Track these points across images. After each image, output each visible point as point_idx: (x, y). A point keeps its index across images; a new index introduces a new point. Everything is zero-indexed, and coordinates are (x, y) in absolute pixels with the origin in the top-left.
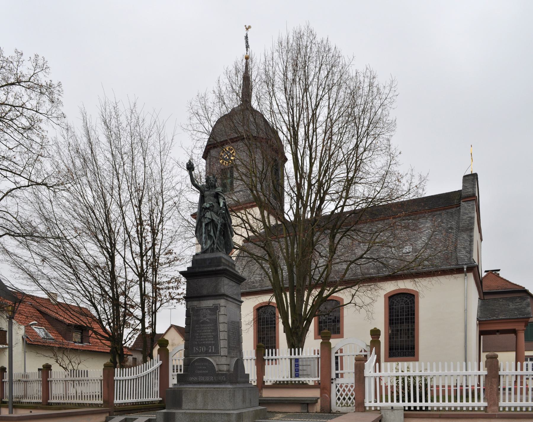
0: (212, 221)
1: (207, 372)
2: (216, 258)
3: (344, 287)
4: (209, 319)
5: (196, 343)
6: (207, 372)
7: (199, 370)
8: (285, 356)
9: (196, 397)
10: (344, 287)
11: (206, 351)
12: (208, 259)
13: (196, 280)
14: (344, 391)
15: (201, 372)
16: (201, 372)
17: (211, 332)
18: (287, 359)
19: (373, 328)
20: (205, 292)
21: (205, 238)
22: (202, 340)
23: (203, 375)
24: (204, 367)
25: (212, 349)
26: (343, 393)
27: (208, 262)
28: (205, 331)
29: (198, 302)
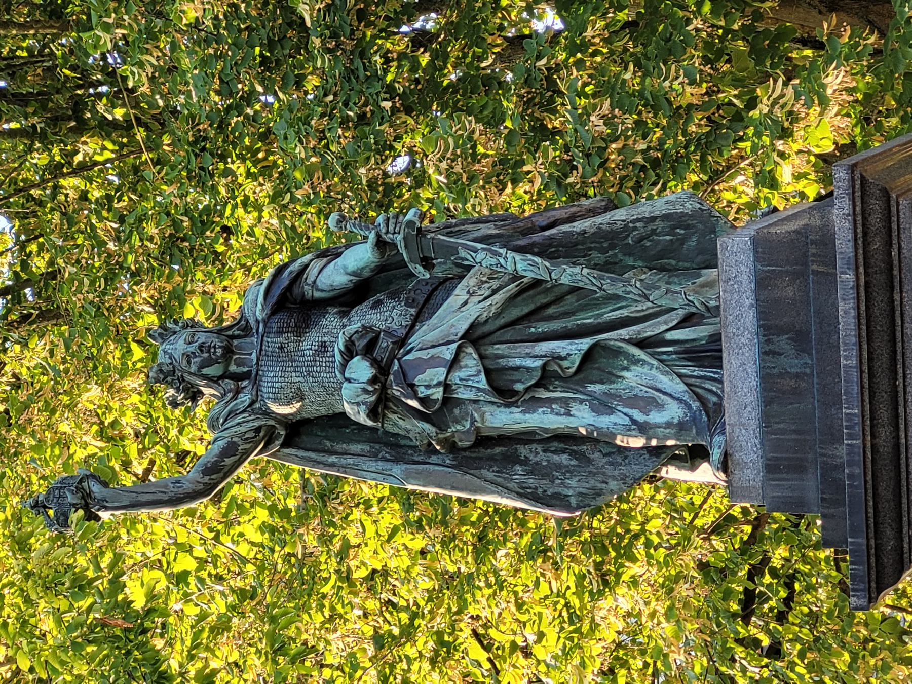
0: (475, 336)
2: (762, 283)
12: (767, 353)
27: (792, 362)
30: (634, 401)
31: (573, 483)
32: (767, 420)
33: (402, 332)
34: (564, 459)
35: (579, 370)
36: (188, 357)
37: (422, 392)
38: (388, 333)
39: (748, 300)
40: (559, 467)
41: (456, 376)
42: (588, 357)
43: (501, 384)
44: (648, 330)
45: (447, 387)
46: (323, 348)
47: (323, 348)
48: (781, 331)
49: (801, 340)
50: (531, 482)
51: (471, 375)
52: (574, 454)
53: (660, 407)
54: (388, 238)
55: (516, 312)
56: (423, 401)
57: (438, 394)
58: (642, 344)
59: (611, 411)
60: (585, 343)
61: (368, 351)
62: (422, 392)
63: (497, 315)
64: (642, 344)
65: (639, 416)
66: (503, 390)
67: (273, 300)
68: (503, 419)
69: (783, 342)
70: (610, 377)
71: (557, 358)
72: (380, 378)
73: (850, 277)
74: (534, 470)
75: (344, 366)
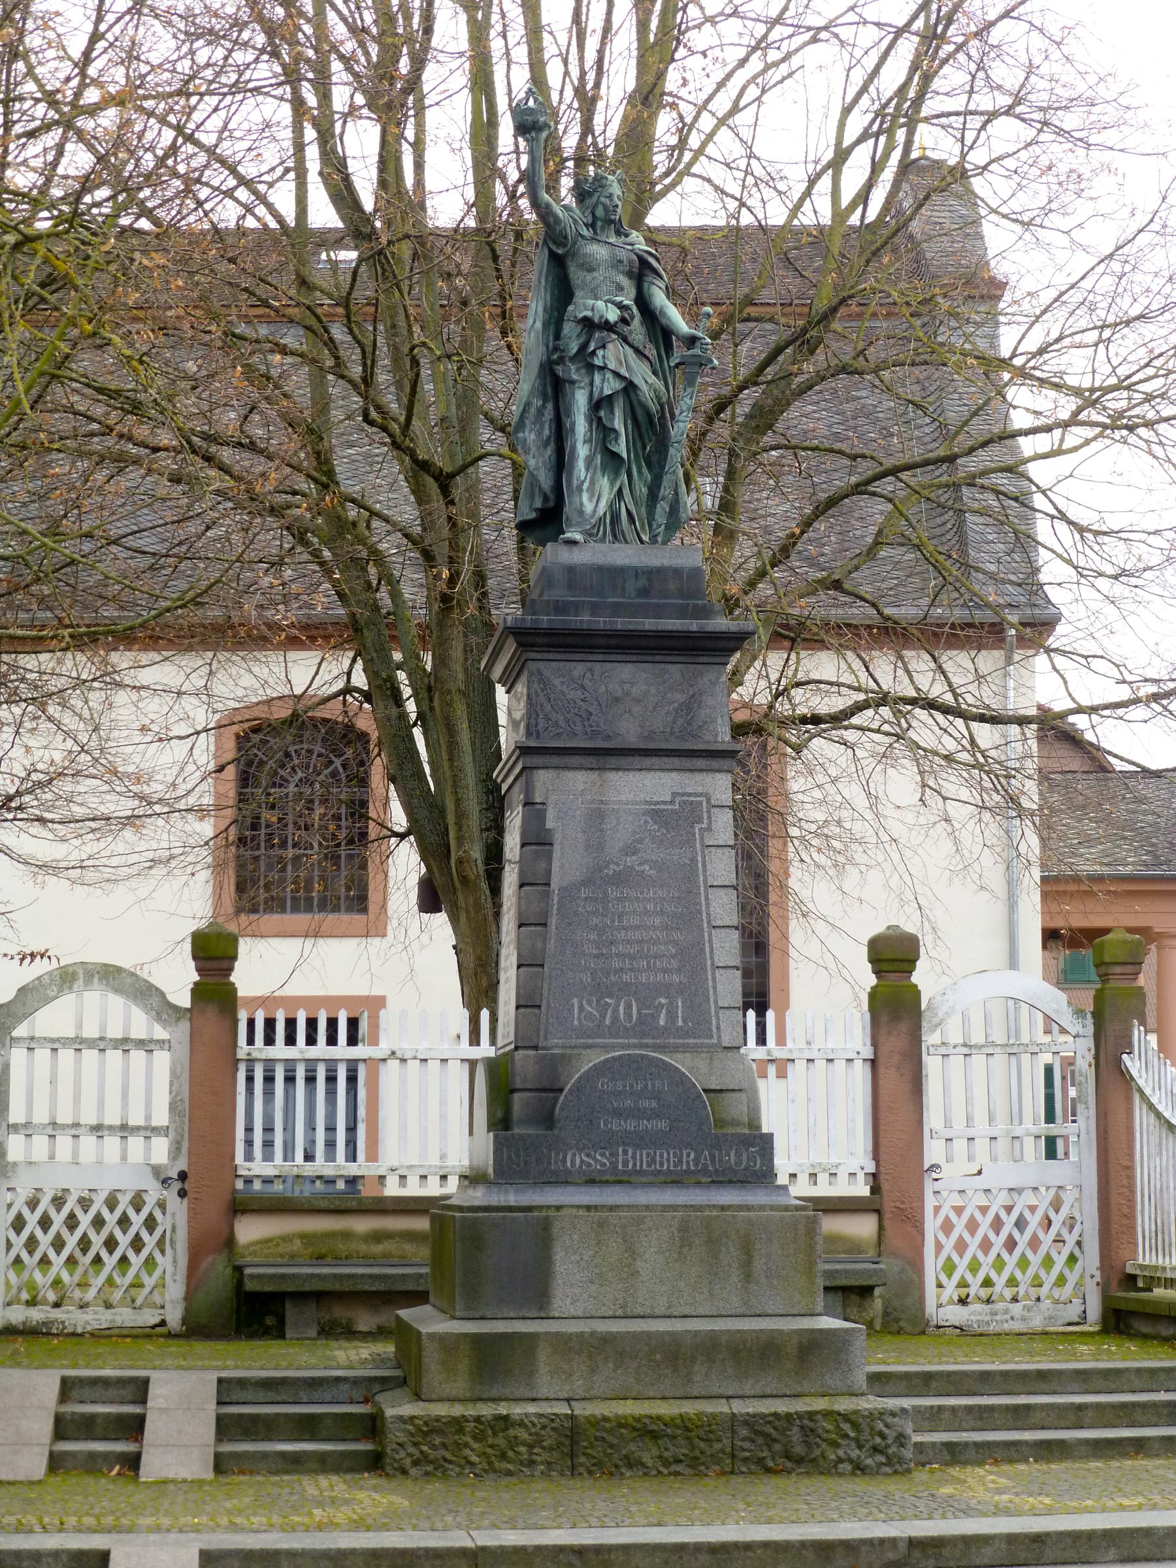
0: (630, 388)
1: (662, 1125)
2: (677, 571)
3: (1110, 758)
4: (654, 865)
5: (586, 978)
6: (662, 1125)
7: (618, 1114)
8: (445, 1048)
9: (632, 1252)
10: (1110, 758)
11: (641, 1021)
12: (637, 572)
13: (579, 669)
14: (45, 1223)
15: (630, 1125)
16: (630, 1125)
17: (666, 927)
18: (858, 1064)
19: (879, 928)
20: (629, 732)
21: (589, 462)
22: (616, 963)
23: (640, 1140)
24: (646, 1104)
25: (671, 1015)
26: (65, 1233)
27: (632, 586)
28: (635, 921)
29: (593, 776)
30: (592, 483)
31: (533, 436)
32: (600, 569)
33: (630, 339)
34: (546, 432)
35: (607, 449)
36: (610, 196)
37: (600, 353)
38: (631, 332)
39: (666, 562)
40: (542, 428)
41: (609, 375)
42: (616, 456)
43: (605, 403)
44: (626, 492)
45: (603, 368)
46: (620, 288)
47: (620, 288)
48: (649, 580)
49: (645, 592)
50: (533, 410)
51: (610, 386)
52: (549, 438)
53: (590, 499)
54: (698, 344)
55: (640, 413)
56: (594, 353)
57: (598, 362)
58: (620, 491)
59: (587, 470)
60: (625, 455)
61: (624, 320)
62: (600, 353)
63: (640, 402)
64: (620, 491)
65: (585, 486)
66: (598, 405)
67: (646, 256)
68: (580, 400)
69: (643, 582)
70: (604, 470)
71: (616, 439)
72: (607, 326)
73: (694, 628)
74: (540, 412)
75: (613, 303)
